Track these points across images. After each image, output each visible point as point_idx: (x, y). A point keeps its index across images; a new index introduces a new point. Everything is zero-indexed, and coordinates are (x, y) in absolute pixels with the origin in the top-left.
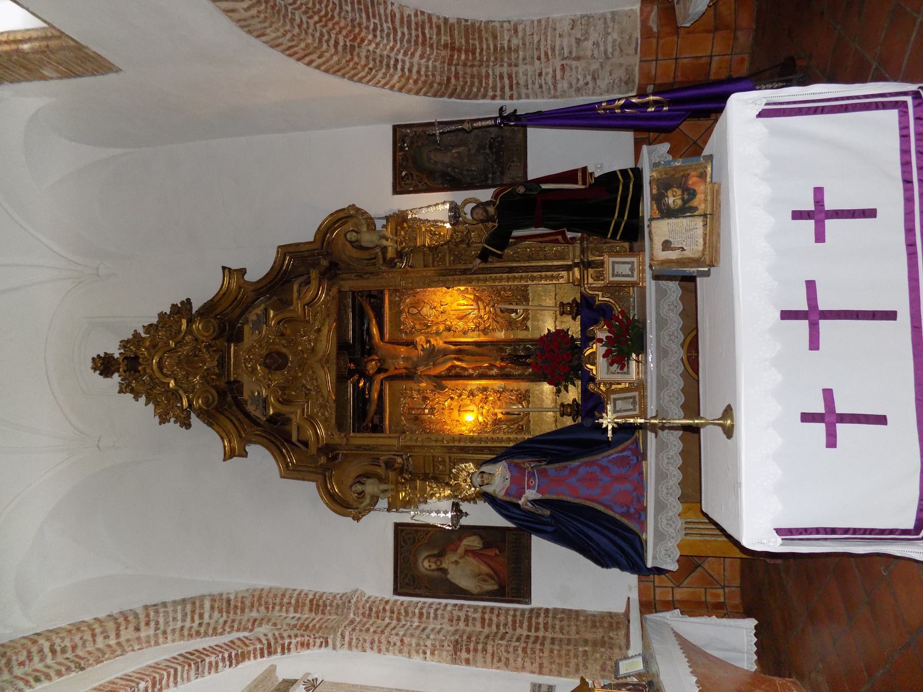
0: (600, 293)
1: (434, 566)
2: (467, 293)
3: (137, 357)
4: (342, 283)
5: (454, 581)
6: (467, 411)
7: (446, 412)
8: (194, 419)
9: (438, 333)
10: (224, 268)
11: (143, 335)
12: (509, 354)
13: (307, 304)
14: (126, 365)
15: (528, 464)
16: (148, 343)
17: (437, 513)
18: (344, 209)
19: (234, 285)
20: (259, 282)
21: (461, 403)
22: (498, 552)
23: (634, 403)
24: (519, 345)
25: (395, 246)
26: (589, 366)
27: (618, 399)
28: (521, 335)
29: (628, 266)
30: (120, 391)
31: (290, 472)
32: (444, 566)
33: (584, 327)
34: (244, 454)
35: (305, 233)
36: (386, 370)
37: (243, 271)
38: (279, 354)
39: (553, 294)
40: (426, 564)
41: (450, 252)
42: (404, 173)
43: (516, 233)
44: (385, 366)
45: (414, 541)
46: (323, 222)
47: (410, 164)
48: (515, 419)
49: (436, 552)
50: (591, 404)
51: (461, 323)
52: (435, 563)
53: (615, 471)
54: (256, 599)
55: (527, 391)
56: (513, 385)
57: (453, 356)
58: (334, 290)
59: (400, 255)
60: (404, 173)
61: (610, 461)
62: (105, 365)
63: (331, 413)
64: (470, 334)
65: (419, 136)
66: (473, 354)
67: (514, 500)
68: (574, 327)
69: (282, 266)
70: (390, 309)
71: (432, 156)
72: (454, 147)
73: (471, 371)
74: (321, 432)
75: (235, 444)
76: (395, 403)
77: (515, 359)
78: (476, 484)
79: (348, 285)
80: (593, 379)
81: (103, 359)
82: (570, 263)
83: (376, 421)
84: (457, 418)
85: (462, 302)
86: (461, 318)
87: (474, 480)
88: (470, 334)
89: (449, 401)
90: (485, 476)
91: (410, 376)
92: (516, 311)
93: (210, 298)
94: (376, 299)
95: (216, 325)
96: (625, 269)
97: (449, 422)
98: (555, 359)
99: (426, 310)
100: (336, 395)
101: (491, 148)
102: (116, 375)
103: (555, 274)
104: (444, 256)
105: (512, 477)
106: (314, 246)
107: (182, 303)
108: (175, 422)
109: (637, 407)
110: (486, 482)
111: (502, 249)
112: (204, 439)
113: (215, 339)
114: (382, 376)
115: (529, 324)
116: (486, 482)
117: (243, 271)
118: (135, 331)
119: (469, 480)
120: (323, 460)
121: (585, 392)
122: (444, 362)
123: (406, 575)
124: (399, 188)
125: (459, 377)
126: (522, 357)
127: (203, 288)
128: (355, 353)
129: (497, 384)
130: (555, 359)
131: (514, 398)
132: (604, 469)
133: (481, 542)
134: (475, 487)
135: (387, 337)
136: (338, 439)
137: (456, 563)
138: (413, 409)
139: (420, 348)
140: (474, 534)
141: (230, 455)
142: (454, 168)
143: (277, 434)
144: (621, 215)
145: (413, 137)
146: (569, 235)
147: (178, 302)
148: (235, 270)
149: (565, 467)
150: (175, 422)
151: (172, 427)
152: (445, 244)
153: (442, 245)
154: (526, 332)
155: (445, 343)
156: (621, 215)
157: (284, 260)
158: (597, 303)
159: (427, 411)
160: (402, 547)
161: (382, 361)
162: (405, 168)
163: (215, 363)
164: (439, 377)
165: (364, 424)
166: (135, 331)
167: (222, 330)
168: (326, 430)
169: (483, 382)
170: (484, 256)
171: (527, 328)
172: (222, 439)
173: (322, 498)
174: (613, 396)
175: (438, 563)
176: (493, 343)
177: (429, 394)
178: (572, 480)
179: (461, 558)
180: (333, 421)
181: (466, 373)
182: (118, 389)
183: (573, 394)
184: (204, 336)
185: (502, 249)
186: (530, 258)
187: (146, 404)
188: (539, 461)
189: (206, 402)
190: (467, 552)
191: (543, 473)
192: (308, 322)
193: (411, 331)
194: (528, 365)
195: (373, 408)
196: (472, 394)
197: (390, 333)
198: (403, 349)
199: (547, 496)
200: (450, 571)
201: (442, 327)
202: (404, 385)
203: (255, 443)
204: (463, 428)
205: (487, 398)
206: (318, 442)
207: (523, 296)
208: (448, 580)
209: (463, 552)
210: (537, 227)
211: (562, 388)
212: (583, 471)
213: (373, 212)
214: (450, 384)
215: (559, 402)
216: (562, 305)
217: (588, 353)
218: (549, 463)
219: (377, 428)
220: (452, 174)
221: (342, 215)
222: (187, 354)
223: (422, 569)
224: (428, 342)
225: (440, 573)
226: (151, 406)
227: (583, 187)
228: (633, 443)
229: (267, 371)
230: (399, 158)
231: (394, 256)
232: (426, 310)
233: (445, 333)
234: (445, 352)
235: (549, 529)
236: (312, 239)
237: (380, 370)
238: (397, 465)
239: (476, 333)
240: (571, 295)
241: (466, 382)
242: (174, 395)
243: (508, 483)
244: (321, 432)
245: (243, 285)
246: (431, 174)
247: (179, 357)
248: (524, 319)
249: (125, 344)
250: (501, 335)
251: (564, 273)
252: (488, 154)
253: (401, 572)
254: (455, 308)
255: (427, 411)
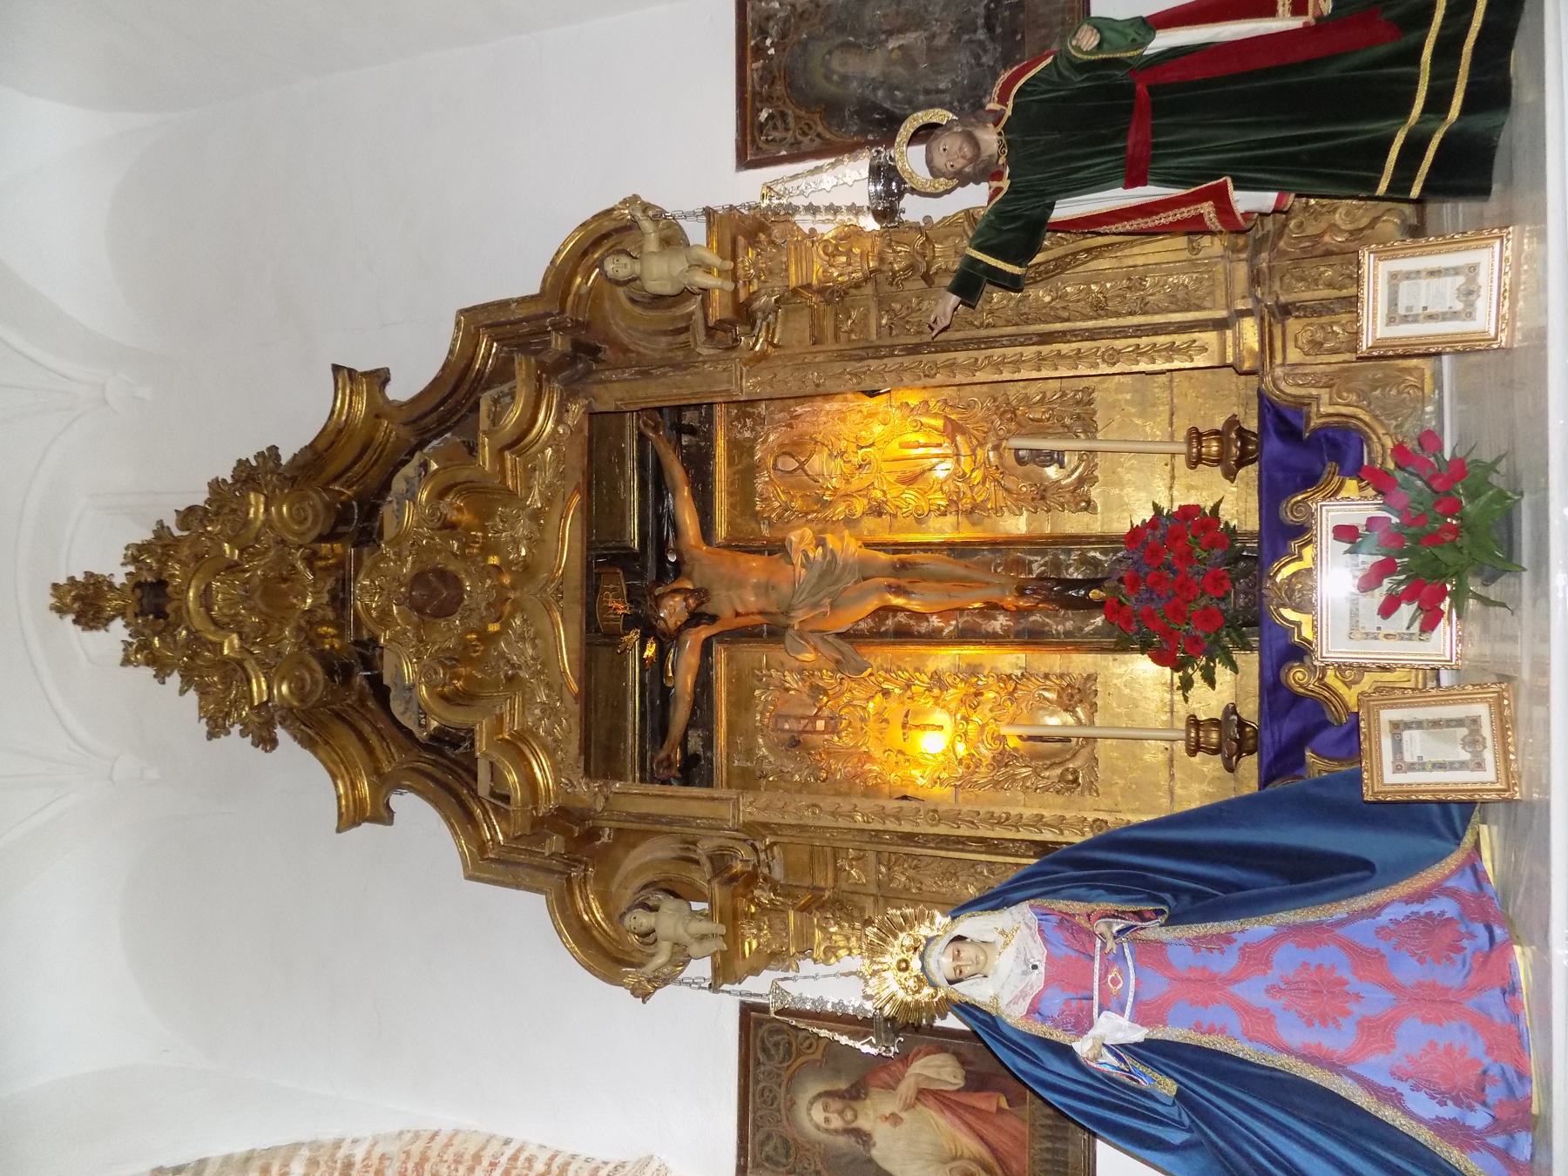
0: (1325, 394)
1: (836, 1123)
2: (927, 413)
3: (161, 584)
4: (595, 389)
5: (887, 1166)
6: (924, 727)
7: (872, 727)
8: (281, 733)
9: (850, 522)
10: (336, 369)
11: (177, 533)
12: (1040, 578)
13: (510, 446)
14: (147, 603)
15: (1103, 918)
16: (185, 551)
17: (842, 979)
18: (609, 212)
19: (361, 407)
20: (413, 401)
21: (909, 705)
22: (1004, 1104)
23: (1473, 741)
24: (1068, 552)
25: (729, 286)
26: (1288, 614)
27: (1408, 726)
28: (1074, 523)
29: (1451, 284)
30: (126, 662)
31: (489, 864)
32: (864, 1123)
33: (1271, 496)
34: (384, 816)
35: (521, 278)
36: (713, 619)
37: (380, 378)
38: (442, 574)
39: (1164, 410)
40: (818, 1114)
41: (880, 303)
42: (764, 115)
43: (1065, 209)
44: (709, 608)
45: (788, 1052)
46: (564, 245)
47: (779, 88)
48: (1054, 754)
49: (843, 1085)
50: (1289, 727)
51: (910, 495)
52: (841, 1113)
53: (1408, 971)
54: (410, 1165)
55: (1091, 678)
56: (1053, 661)
57: (885, 581)
58: (576, 409)
59: (744, 313)
60: (764, 115)
61: (1381, 931)
62: (85, 602)
63: (567, 729)
64: (935, 522)
65: (801, 15)
66: (940, 579)
67: (1059, 1036)
68: (1236, 502)
69: (473, 359)
70: (731, 462)
71: (835, 63)
72: (890, 33)
73: (936, 621)
74: (542, 771)
75: (365, 788)
76: (742, 703)
77: (1062, 593)
78: (940, 979)
79: (614, 392)
80: (1299, 652)
81: (85, 586)
82: (1223, 314)
83: (695, 744)
84: (900, 744)
85: (912, 437)
86: (910, 480)
87: (932, 964)
88: (935, 522)
89: (879, 697)
90: (967, 952)
91: (772, 631)
92: (1055, 458)
93: (307, 443)
94: (686, 427)
95: (320, 506)
96: (1445, 293)
97: (877, 753)
98: (1187, 592)
99: (818, 463)
100: (579, 682)
101: (990, 28)
102: (118, 623)
103: (1180, 339)
104: (866, 316)
105: (1050, 960)
106: (539, 309)
107: (260, 455)
108: (243, 734)
109: (1488, 755)
110: (967, 970)
111: (1022, 257)
112: (298, 776)
113: (322, 538)
114: (704, 632)
115: (1095, 493)
116: (967, 970)
117: (380, 378)
118: (160, 523)
119: (916, 964)
120: (555, 843)
121: (1273, 691)
122: (863, 596)
123: (769, 1137)
124: (751, 152)
125: (903, 635)
126: (1076, 584)
127: (295, 420)
128: (631, 570)
129: (1010, 660)
130: (1187, 592)
131: (1052, 696)
132: (1363, 958)
133: (960, 1073)
134: (935, 986)
135: (721, 531)
136: (585, 791)
137: (895, 1119)
138: (787, 717)
139: (798, 558)
140: (941, 1049)
141: (352, 816)
142: (891, 88)
143: (446, 769)
144: (1439, 102)
145: (786, 20)
146: (1245, 201)
147: (249, 454)
148: (365, 374)
149: (1227, 939)
150: (243, 734)
151: (236, 743)
152: (866, 279)
153: (857, 286)
154: (1085, 517)
155: (867, 545)
156: (1439, 102)
157: (477, 345)
158: (1315, 422)
159: (820, 724)
160: (758, 1063)
161: (702, 594)
162: (768, 100)
163: (326, 598)
164: (850, 636)
165: (662, 755)
166: (160, 523)
167: (343, 517)
168: (557, 769)
169: (971, 652)
170: (969, 284)
171: (1089, 506)
172: (334, 777)
173: (560, 933)
174: (1387, 715)
175: (849, 1115)
176: (994, 545)
177: (827, 679)
178: (1252, 991)
179: (909, 1107)
180: (574, 747)
181: (923, 627)
182: (121, 655)
183: (1230, 688)
184: (295, 534)
185: (1022, 257)
186: (1100, 309)
187: (182, 692)
188: (1140, 915)
189: (299, 690)
190: (925, 1094)
191: (1151, 953)
192: (512, 494)
193: (780, 517)
194: (1091, 606)
195: (680, 715)
196: (938, 681)
197: (730, 524)
198: (755, 562)
199: (1160, 1034)
200: (877, 1138)
201: (860, 506)
202: (758, 655)
203: (411, 789)
204: (916, 773)
205: (978, 694)
206: (535, 802)
207: (1080, 415)
208: (870, 1161)
209: (912, 1093)
210: (1131, 183)
211: (1197, 676)
212: (1288, 959)
213: (670, 206)
214: (879, 656)
215: (1182, 710)
216: (1196, 436)
217: (1286, 572)
218: (1174, 920)
219: (693, 770)
220: (887, 105)
221: (608, 225)
222: (265, 578)
223: (808, 1127)
224: (821, 543)
225: (853, 1140)
226: (192, 696)
227: (1296, 23)
228: (1460, 870)
229: (415, 617)
230: (753, 76)
231: (728, 314)
232: (818, 462)
233: (870, 523)
234: (865, 573)
235: (1177, 1137)
236: (536, 290)
237: (696, 618)
238: (738, 867)
239: (951, 519)
240: (1231, 405)
241: (923, 650)
242: (233, 671)
243: (1037, 979)
244: (542, 771)
245: (380, 408)
246: (831, 109)
247: (246, 582)
248: (1081, 481)
249: (136, 554)
250: (1017, 525)
251: (1210, 337)
252: (981, 43)
253: (757, 1128)
254: (891, 454)
255: (820, 724)
